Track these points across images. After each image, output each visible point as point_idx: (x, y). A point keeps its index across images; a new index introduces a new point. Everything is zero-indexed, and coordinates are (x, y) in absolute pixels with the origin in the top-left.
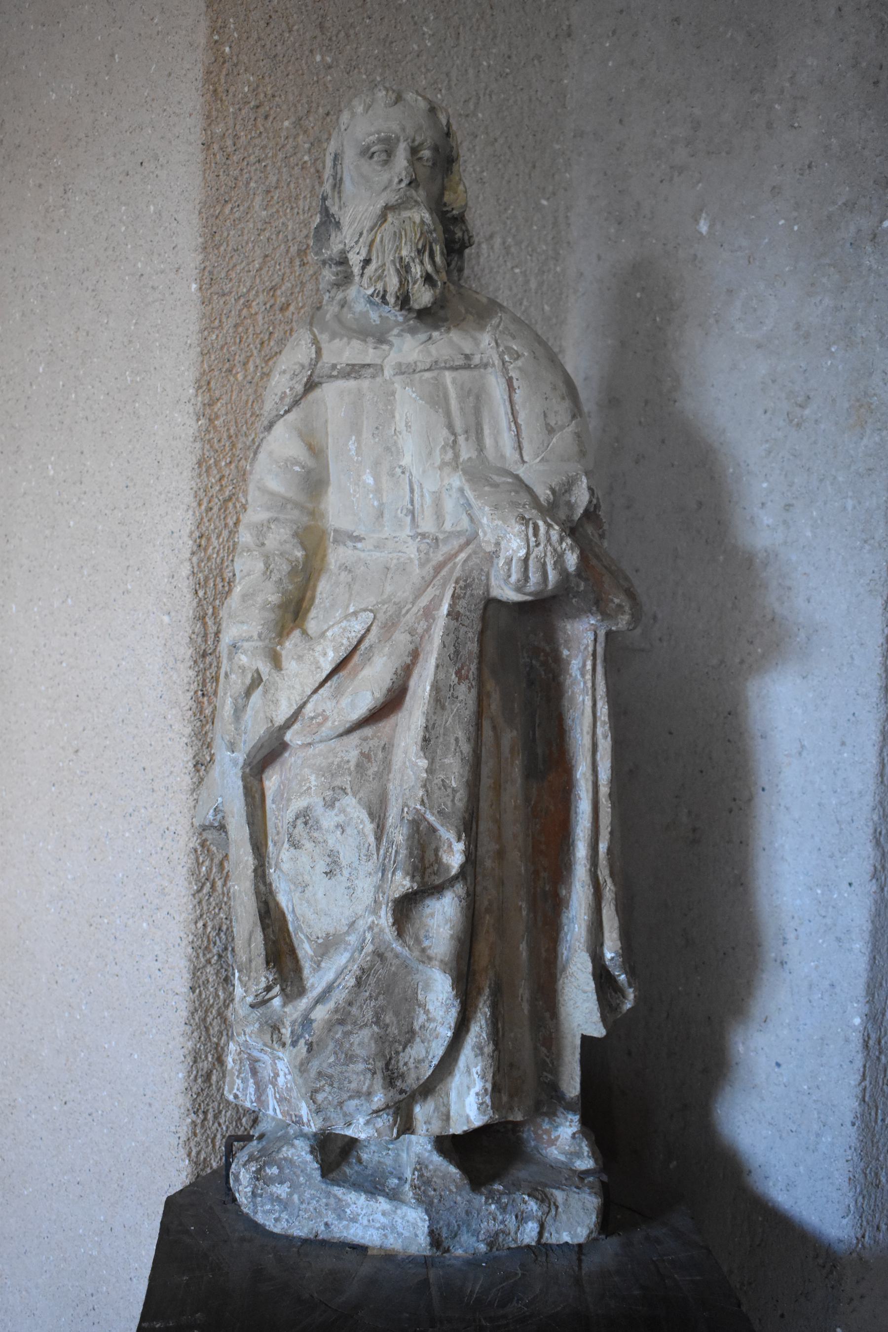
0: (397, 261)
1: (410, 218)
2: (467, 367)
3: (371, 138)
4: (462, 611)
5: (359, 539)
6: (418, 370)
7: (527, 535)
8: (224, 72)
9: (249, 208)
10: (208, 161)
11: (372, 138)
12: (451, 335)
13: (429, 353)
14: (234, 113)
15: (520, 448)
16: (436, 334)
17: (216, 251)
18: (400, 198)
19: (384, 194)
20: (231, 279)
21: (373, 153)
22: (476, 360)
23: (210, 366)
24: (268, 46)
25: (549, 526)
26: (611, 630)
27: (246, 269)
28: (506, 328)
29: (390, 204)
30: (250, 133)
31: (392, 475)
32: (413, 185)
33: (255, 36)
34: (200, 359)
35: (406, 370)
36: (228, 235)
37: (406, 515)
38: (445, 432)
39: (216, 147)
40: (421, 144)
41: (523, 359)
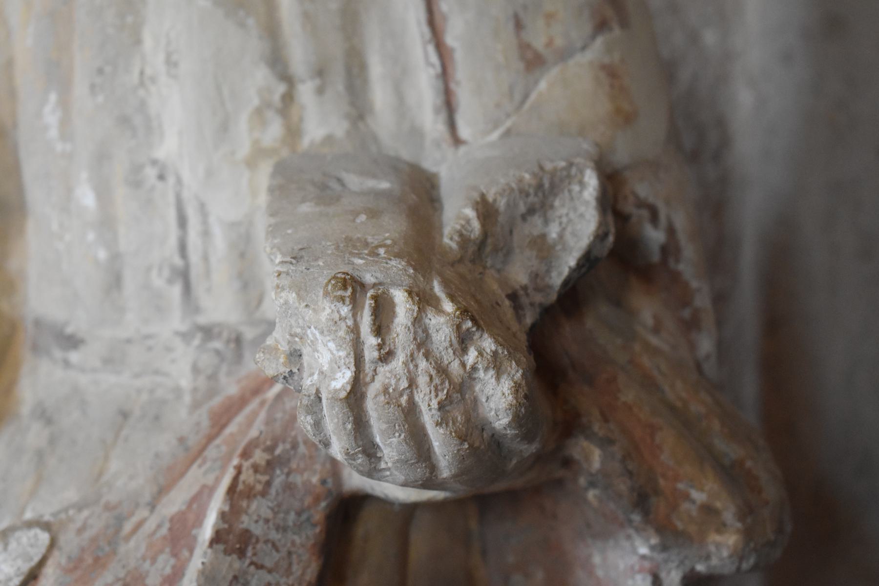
4: (257, 530)
5: (72, 342)
7: (355, 330)
15: (449, 106)
25: (423, 300)
26: (693, 570)
31: (135, 182)
37: (170, 281)
38: (262, 75)
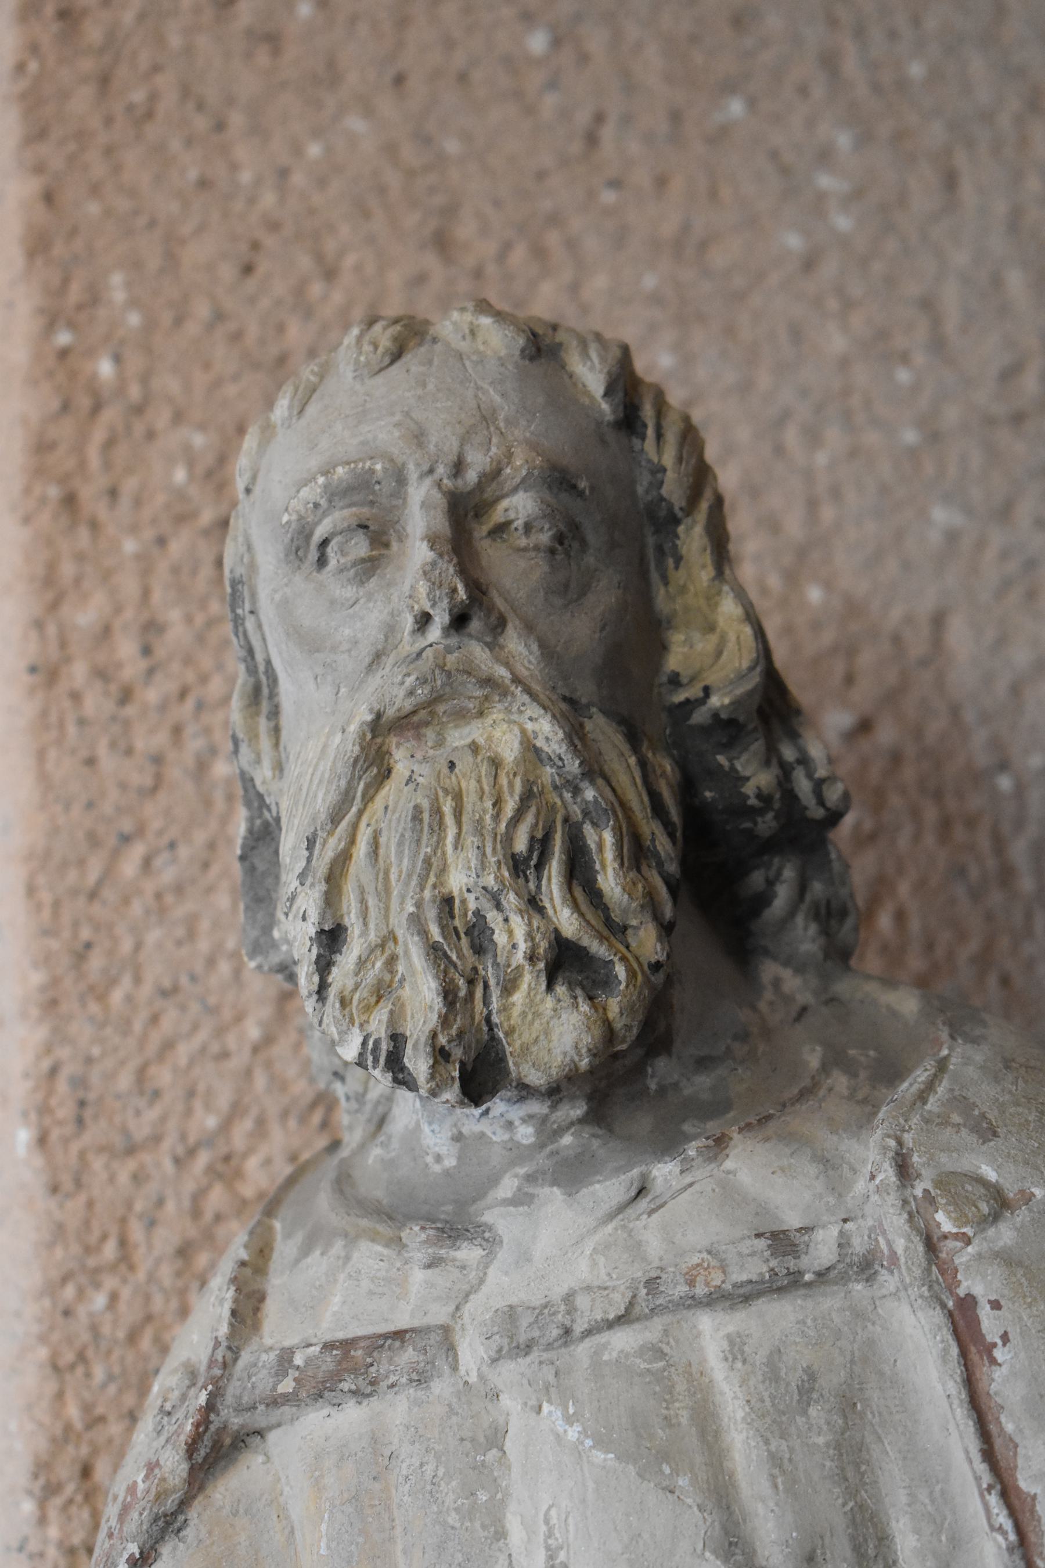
0: (431, 914)
1: (474, 748)
2: (786, 1283)
3: (305, 492)
6: (578, 1328)
8: (98, 435)
9: (212, 846)
10: (53, 718)
11: (310, 493)
12: (729, 1164)
13: (636, 1249)
14: (139, 557)
16: (664, 1172)
17: (94, 1008)
18: (423, 681)
19: (375, 681)
20: (157, 1094)
21: (324, 543)
22: (823, 1250)
23: (87, 1408)
24: (253, 331)
27: (215, 1048)
28: (960, 1102)
29: (390, 713)
30: (203, 603)
32: (475, 625)
33: (202, 310)
34: (51, 1387)
35: (538, 1335)
36: (138, 946)
39: (79, 672)
40: (494, 474)
41: (1022, 1215)
